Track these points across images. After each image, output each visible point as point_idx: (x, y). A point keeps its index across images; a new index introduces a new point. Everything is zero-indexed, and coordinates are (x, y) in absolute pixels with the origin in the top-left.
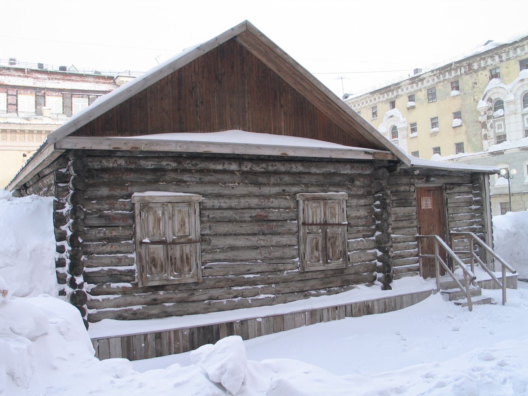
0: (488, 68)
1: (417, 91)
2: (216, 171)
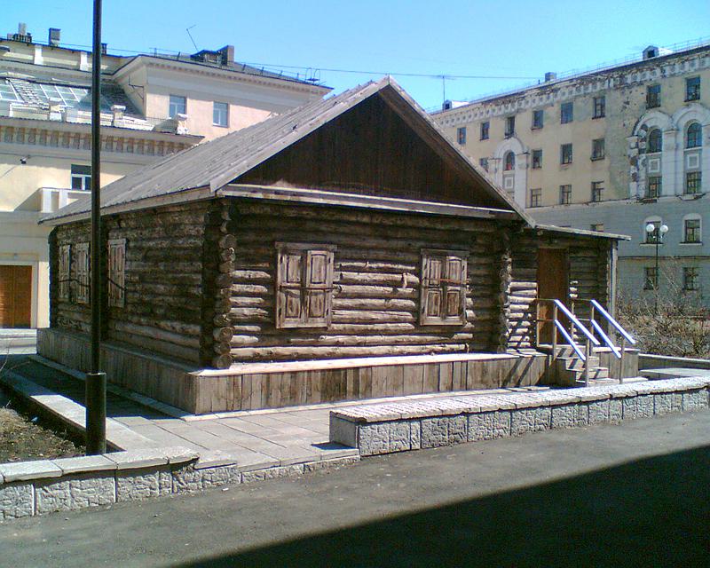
0: (646, 84)
1: (546, 106)
2: (349, 223)
